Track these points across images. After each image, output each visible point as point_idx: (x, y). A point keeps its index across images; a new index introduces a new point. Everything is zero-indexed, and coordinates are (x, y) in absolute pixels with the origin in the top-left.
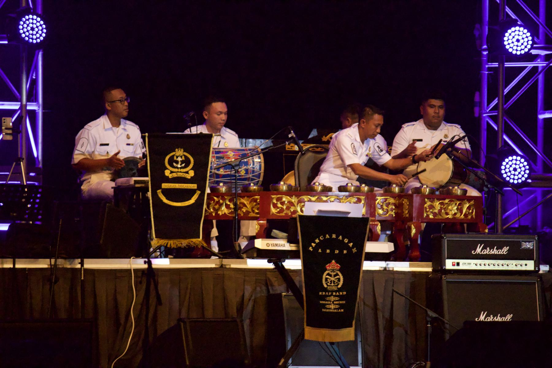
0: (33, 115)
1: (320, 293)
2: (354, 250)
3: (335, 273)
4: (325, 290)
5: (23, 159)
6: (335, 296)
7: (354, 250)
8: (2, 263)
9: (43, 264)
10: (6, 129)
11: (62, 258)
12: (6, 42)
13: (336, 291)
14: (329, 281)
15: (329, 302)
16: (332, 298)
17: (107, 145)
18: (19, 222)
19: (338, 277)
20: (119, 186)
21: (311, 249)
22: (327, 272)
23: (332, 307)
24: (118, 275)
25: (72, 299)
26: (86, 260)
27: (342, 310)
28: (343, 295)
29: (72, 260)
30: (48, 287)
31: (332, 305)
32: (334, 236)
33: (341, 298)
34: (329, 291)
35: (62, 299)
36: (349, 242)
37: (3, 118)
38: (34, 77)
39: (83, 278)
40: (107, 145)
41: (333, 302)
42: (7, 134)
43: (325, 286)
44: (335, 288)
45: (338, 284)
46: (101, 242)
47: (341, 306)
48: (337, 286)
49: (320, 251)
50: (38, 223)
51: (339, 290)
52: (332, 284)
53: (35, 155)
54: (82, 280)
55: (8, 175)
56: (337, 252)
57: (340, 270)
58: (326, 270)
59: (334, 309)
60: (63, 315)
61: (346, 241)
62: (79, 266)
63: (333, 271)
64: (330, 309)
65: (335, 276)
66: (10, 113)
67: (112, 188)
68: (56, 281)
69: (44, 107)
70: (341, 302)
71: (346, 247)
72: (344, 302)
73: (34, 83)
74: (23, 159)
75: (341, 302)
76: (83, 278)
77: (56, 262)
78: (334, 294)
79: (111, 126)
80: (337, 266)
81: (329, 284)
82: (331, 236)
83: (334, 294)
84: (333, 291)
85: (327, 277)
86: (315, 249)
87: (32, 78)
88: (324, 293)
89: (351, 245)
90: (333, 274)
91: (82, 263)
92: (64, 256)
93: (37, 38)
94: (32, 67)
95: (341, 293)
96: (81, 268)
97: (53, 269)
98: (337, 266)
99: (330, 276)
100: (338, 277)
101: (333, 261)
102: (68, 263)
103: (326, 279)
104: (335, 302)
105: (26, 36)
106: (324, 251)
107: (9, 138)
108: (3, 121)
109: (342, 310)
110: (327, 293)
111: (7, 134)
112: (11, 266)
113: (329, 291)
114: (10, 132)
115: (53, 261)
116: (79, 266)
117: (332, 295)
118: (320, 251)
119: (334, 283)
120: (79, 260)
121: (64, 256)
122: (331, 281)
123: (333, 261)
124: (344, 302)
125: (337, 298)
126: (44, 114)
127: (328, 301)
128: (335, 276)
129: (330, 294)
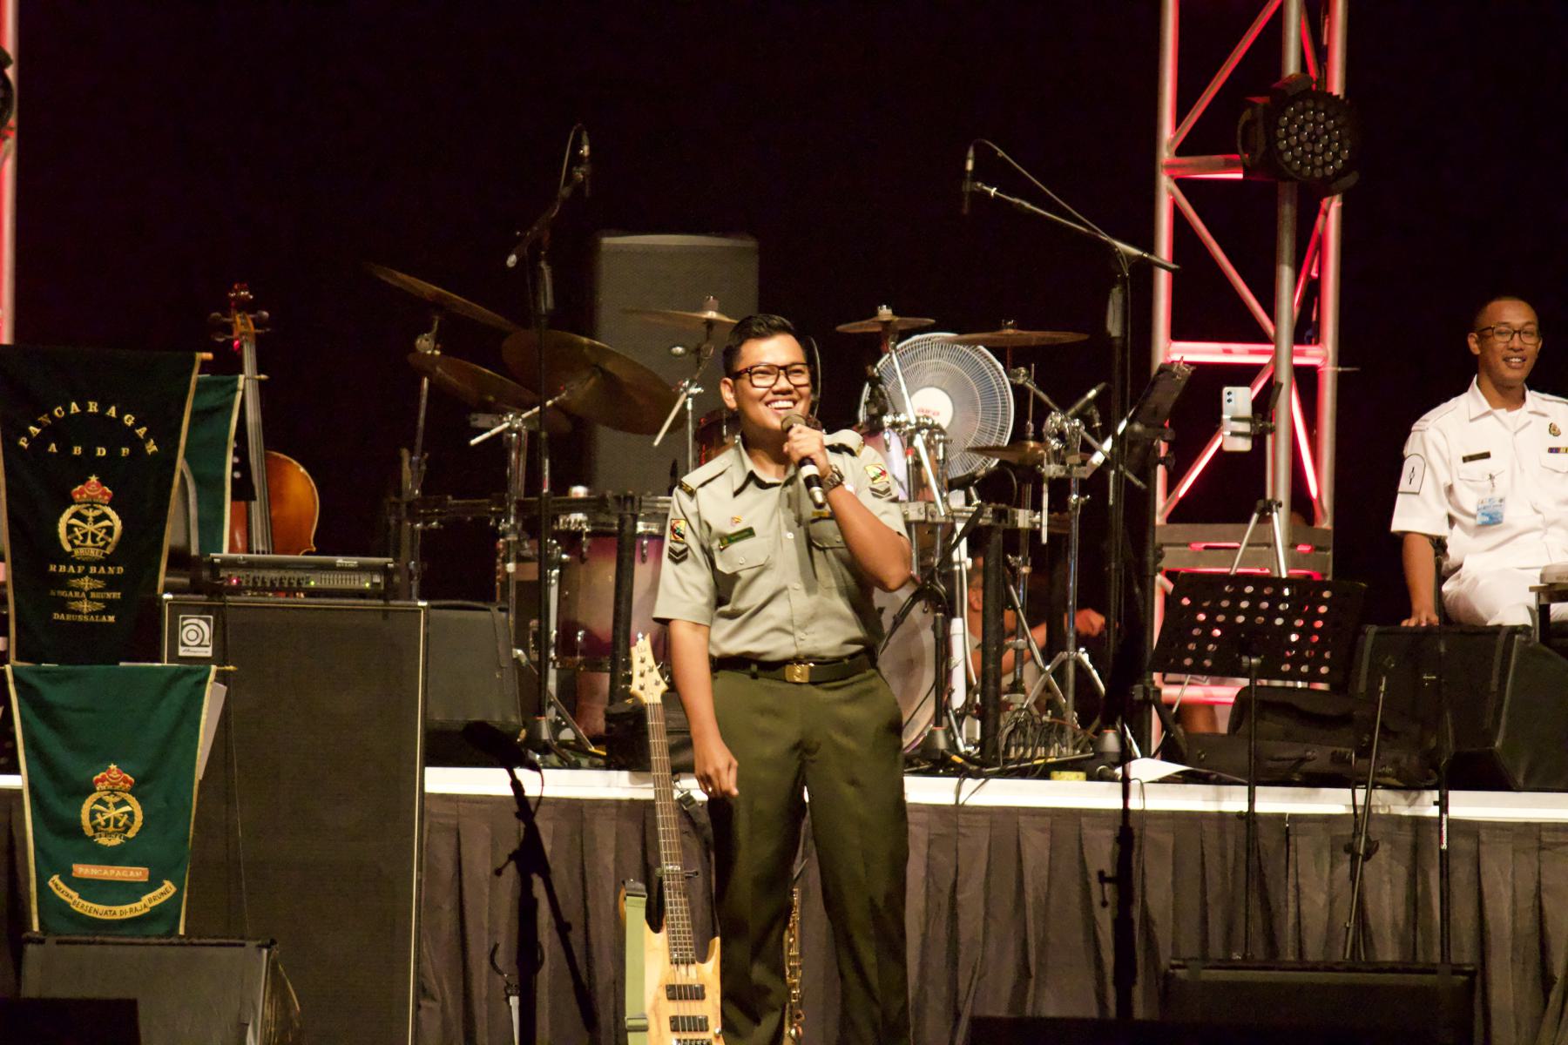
0: (1307, 379)
1: (53, 568)
2: (151, 448)
3: (97, 513)
4: (67, 559)
5: (1280, 505)
6: (94, 576)
7: (151, 448)
8: (1219, 799)
9: (1334, 802)
10: (1233, 419)
11: (1387, 787)
12: (1240, 176)
13: (98, 563)
14: (78, 533)
15: (77, 594)
16: (86, 583)
17: (1486, 455)
18: (1265, 682)
19: (127, 808)
20: (1551, 585)
21: (23, 443)
22: (73, 509)
23: (85, 606)
24: (1547, 838)
25: (1415, 903)
26: (1454, 795)
27: (112, 619)
28: (115, 576)
29: (1414, 794)
30: (1345, 868)
31: (87, 602)
32: (93, 407)
33: (111, 583)
34: (76, 563)
35: (1387, 900)
36: (137, 424)
37: (1226, 389)
38: (1314, 274)
39: (1444, 846)
40: (1486, 455)
41: (88, 594)
42: (1235, 434)
43: (68, 548)
44: (94, 553)
45: (107, 544)
46: (1498, 744)
47: (110, 606)
48: (104, 548)
49: (53, 448)
50: (1322, 686)
51: (107, 561)
52: (89, 542)
53: (1314, 493)
54: (1441, 851)
55: (1236, 548)
56: (101, 452)
57: (112, 505)
58: (72, 502)
59: (89, 614)
60: (1388, 952)
61: (129, 420)
62: (1434, 812)
63: (92, 504)
64: (78, 612)
65: (97, 520)
66: (1241, 376)
67: (1531, 589)
68: (1368, 856)
69: (1343, 357)
70: (109, 595)
71: (128, 436)
72: (117, 595)
73: (1313, 292)
74: (1280, 505)
75: (109, 595)
76: (1444, 846)
77: (1368, 798)
78: (93, 570)
79: (1487, 407)
80: (125, 780)
81: (77, 542)
82: (83, 407)
83: (93, 570)
84: (87, 563)
85: (74, 521)
86: (38, 443)
87: (1309, 275)
88: (62, 568)
89: (141, 432)
90: (91, 514)
91: (1443, 804)
92: (1394, 782)
93: (1325, 164)
94: (1307, 243)
95: (111, 570)
96: (1441, 818)
97: (1361, 819)
98: (104, 493)
99: (105, 804)
100: (106, 523)
101: (94, 479)
102: (1403, 801)
103: (70, 528)
104: (93, 595)
105: (1295, 158)
106: (65, 449)
107: (1244, 445)
108: (1225, 397)
109: (112, 619)
110: (72, 569)
111: (1235, 434)
112: (1245, 808)
113: (76, 563)
114: (1244, 427)
115: (1361, 794)
116: (1434, 812)
117: (86, 573)
118: (53, 448)
119: (94, 541)
120: (1436, 795)
121: (1394, 782)
122: (85, 535)
123: (94, 479)
124: (117, 595)
125: (100, 584)
126: (1342, 381)
127: (73, 589)
128: (97, 520)
129: (80, 569)
